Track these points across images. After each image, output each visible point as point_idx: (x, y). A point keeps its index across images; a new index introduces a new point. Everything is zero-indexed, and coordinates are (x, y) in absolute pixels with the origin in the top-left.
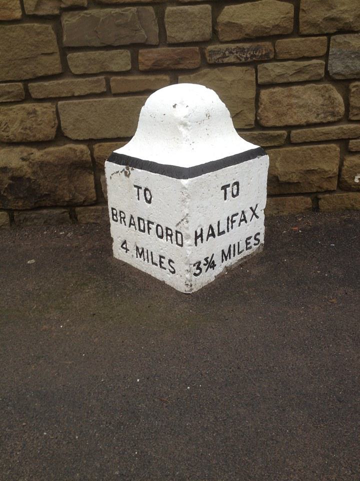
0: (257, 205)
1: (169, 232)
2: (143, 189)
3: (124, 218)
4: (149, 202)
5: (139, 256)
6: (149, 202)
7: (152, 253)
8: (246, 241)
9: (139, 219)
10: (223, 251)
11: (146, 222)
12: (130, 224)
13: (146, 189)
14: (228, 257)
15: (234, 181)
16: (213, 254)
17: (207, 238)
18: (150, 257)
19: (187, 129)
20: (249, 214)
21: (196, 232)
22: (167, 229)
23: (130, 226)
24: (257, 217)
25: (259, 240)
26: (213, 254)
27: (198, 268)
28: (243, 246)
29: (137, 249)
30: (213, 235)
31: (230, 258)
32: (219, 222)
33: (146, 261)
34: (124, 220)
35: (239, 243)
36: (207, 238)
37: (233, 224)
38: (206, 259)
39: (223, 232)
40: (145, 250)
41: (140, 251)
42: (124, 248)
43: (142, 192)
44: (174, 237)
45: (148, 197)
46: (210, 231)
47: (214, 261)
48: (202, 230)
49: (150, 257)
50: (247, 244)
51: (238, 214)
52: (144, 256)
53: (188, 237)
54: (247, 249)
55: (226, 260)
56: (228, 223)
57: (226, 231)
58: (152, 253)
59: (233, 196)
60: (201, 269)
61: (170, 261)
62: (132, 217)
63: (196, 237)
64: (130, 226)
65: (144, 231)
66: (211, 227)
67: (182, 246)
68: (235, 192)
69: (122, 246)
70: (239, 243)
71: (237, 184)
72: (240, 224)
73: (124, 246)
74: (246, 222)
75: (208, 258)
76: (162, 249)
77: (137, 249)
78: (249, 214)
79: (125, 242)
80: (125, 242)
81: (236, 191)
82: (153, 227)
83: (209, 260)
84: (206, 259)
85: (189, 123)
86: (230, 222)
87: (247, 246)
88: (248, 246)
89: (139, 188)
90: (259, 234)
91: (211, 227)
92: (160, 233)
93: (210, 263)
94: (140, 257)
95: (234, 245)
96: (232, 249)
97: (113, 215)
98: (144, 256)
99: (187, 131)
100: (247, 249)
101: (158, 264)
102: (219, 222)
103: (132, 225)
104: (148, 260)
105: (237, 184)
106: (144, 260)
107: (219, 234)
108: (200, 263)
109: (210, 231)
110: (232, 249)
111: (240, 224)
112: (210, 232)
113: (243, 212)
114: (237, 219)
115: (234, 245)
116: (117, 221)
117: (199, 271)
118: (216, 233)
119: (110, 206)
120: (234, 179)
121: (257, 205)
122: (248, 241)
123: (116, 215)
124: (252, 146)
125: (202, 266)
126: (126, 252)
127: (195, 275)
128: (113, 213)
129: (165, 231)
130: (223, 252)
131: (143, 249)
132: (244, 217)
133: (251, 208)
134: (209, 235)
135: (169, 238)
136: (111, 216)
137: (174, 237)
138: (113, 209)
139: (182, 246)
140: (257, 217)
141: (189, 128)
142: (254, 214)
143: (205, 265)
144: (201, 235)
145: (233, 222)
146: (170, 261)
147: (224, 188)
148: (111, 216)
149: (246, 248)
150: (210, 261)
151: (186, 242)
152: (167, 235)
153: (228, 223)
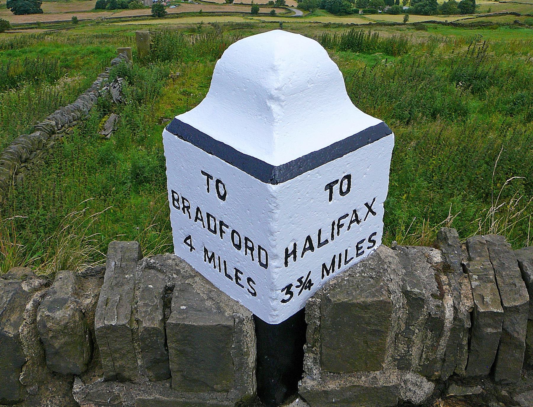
0: (374, 199)
1: (250, 244)
2: (215, 180)
3: (188, 207)
4: (223, 198)
5: (207, 259)
6: (223, 198)
7: (225, 262)
8: (357, 246)
9: (208, 215)
10: (324, 266)
11: (218, 223)
12: (197, 218)
13: (218, 181)
14: (331, 271)
15: (346, 174)
16: (310, 272)
17: (303, 254)
18: (223, 267)
19: (281, 106)
20: (362, 212)
21: (287, 250)
22: (246, 239)
23: (196, 221)
24: (374, 213)
25: (374, 242)
26: (310, 272)
27: (289, 292)
28: (352, 252)
29: (206, 251)
30: (311, 248)
31: (333, 270)
32: (320, 231)
33: (217, 269)
34: (188, 210)
35: (346, 251)
36: (303, 254)
37: (340, 229)
38: (300, 280)
39: (327, 241)
40: (216, 256)
41: (210, 255)
42: (187, 243)
43: (212, 183)
44: (256, 252)
45: (222, 193)
46: (308, 243)
47: (310, 280)
48: (295, 245)
49: (223, 267)
50: (358, 249)
51: (347, 215)
52: (287, 13)
53: (276, 256)
54: (358, 255)
55: (328, 275)
56: (333, 229)
57: (329, 239)
58: (225, 262)
59: (342, 193)
60: (291, 294)
61: (249, 280)
62: (198, 209)
63: (287, 256)
64: (196, 221)
65: (215, 232)
66: (309, 239)
67: (266, 266)
68: (344, 189)
69: (185, 241)
70: (346, 251)
71: (348, 177)
72: (349, 227)
73: (188, 241)
74: (358, 222)
75: (303, 277)
76: (238, 262)
77: (206, 251)
78: (362, 212)
79: (189, 237)
80: (189, 237)
81: (347, 186)
82: (228, 231)
83: (303, 280)
84: (300, 280)
85: (283, 98)
86: (336, 227)
87: (357, 252)
88: (359, 252)
89: (209, 177)
90: (375, 234)
91: (309, 239)
92: (237, 242)
93: (305, 283)
94: (210, 263)
95: (340, 255)
96: (337, 260)
97: (174, 199)
98: (287, 13)
99: (279, 107)
100: (358, 255)
101: (234, 278)
102: (320, 231)
103: (199, 219)
104: (220, 269)
105: (348, 177)
106: (215, 267)
107: (320, 245)
108: (291, 285)
109: (308, 243)
110: (337, 260)
111: (349, 227)
112: (308, 245)
113: (355, 211)
114: (346, 221)
115: (340, 255)
116: (179, 208)
117: (289, 296)
118: (315, 244)
119: (170, 187)
120: (344, 173)
121: (374, 199)
122: (360, 246)
123: (178, 200)
124: (375, 121)
125: (293, 289)
126: (191, 250)
127: (284, 301)
128: (173, 196)
129: (243, 241)
130: (324, 266)
131: (213, 253)
132: (356, 216)
133: (366, 204)
134: (305, 250)
135: (249, 251)
136: (170, 199)
137: (256, 252)
138: (173, 192)
139: (266, 266)
140: (374, 213)
141: (283, 104)
142: (370, 210)
143: (297, 287)
144: (294, 252)
145: (340, 226)
146: (249, 280)
147: (330, 187)
148: (170, 199)
149: (357, 254)
150: (306, 281)
151: (272, 263)
152: (247, 247)
153: (333, 229)
